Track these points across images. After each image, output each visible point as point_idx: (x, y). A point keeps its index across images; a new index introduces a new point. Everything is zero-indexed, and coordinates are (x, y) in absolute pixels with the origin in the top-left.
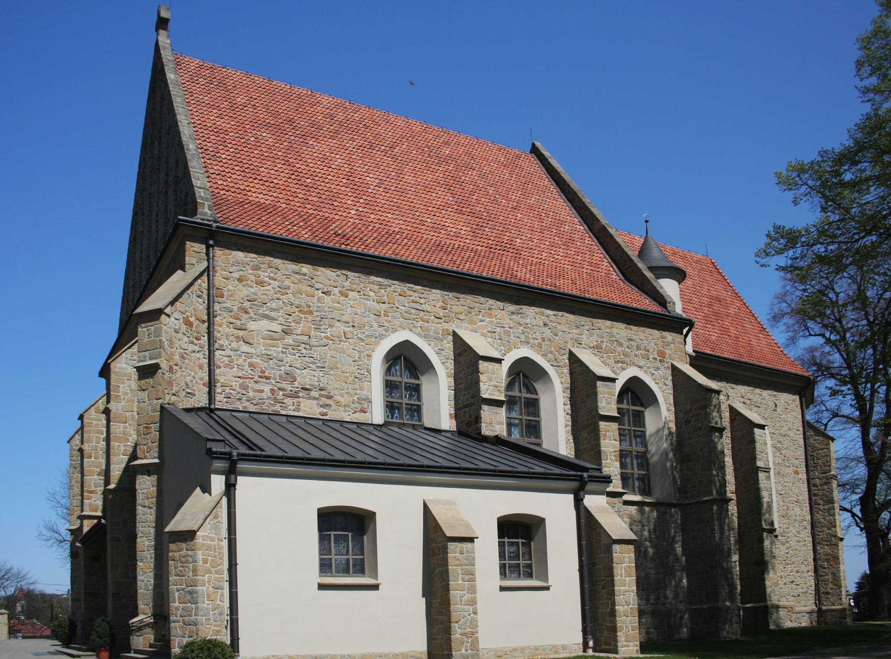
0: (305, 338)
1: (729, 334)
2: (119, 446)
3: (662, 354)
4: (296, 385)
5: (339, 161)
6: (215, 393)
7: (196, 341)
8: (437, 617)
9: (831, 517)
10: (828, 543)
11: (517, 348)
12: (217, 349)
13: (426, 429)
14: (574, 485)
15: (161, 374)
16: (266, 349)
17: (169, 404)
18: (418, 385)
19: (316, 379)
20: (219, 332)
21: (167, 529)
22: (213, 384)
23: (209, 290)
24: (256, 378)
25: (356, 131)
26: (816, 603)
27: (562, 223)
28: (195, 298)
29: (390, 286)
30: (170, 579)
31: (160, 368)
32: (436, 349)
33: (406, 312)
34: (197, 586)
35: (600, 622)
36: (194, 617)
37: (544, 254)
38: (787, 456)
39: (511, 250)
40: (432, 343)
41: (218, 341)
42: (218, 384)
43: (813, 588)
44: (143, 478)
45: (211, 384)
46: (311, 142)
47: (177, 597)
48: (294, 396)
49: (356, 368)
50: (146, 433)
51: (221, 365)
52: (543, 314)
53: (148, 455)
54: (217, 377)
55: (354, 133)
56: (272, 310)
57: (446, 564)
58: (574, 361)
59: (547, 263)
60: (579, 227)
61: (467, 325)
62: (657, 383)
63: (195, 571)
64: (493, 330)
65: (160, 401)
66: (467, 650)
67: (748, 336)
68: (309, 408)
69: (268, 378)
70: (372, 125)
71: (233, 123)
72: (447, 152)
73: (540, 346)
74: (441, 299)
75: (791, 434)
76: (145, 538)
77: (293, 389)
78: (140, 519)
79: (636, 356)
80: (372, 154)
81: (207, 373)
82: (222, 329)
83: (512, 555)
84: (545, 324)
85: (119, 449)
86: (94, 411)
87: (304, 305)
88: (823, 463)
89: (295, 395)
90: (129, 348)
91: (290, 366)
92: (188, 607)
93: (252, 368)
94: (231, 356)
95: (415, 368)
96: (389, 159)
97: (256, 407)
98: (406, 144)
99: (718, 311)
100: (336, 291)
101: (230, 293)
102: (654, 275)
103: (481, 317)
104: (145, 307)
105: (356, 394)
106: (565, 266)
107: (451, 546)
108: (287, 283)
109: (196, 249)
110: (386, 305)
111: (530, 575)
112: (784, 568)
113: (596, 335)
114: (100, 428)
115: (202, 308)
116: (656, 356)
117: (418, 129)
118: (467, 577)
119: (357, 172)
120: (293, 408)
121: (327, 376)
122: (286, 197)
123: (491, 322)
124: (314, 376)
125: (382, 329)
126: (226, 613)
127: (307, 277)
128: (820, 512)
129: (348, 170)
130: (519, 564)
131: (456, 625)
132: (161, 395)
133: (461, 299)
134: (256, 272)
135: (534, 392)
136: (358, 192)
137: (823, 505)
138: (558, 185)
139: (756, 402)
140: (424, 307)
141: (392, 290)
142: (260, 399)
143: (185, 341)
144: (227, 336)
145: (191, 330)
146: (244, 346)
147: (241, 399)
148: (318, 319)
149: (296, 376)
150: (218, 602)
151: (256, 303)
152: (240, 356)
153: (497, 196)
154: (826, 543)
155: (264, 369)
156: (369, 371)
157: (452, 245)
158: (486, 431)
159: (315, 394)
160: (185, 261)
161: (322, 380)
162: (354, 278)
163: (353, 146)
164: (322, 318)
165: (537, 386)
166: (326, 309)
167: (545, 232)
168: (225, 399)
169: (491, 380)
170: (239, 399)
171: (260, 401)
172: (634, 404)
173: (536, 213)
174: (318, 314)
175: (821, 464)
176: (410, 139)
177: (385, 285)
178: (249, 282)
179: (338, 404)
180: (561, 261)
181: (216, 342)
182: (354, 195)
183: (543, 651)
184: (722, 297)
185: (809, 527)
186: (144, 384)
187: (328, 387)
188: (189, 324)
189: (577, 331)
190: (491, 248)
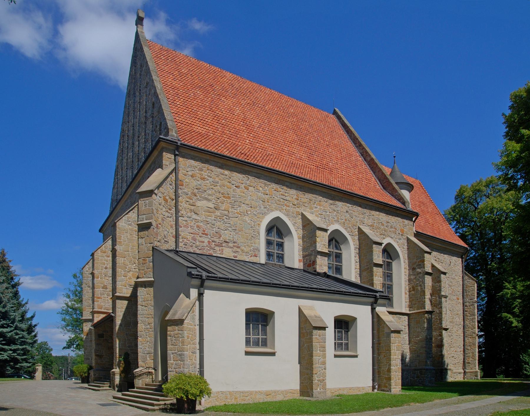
0: (226, 213)
1: (429, 222)
2: (121, 271)
3: (402, 231)
4: (221, 239)
5: (238, 111)
6: (179, 242)
7: (169, 211)
8: (304, 371)
9: (473, 323)
10: (471, 337)
11: (333, 224)
12: (180, 216)
13: (286, 267)
14: (372, 300)
15: (152, 229)
16: (206, 218)
17: (156, 247)
18: (283, 243)
19: (231, 236)
20: (181, 206)
21: (167, 318)
22: (178, 237)
24: (201, 234)
25: (245, 94)
27: (351, 155)
28: (169, 186)
30: (168, 347)
31: (152, 225)
32: (293, 222)
33: (278, 201)
34: (184, 351)
35: (381, 375)
36: (182, 369)
37: (344, 172)
38: (454, 290)
39: (328, 169)
40: (291, 219)
41: (180, 212)
42: (180, 237)
44: (142, 289)
45: (177, 236)
46: (223, 99)
47: (172, 357)
48: (220, 246)
49: (252, 231)
50: (143, 263)
51: (182, 226)
52: (346, 206)
54: (180, 233)
55: (244, 96)
56: (209, 195)
57: (312, 342)
58: (361, 232)
59: (346, 177)
60: (359, 158)
61: (308, 209)
62: (399, 247)
63: (183, 342)
64: (321, 213)
65: (152, 245)
66: (320, 389)
67: (438, 224)
68: (228, 253)
69: (207, 235)
70: (253, 92)
71: (181, 84)
72: (292, 111)
73: (344, 223)
74: (296, 194)
75: (457, 278)
76: (143, 324)
77: (220, 242)
79: (390, 231)
80: (255, 109)
81: (175, 230)
82: (183, 204)
83: (339, 338)
84: (347, 211)
85: (121, 273)
86: (100, 251)
87: (226, 194)
88: (471, 294)
89: (220, 245)
90: (127, 214)
91: (218, 228)
92: (178, 363)
93: (198, 229)
94: (187, 221)
95: (282, 234)
96: (263, 112)
98: (271, 104)
99: (423, 210)
100: (243, 186)
101: (187, 184)
102: (399, 187)
103: (315, 205)
104: (143, 188)
105: (252, 246)
106: (354, 179)
107: (315, 332)
108: (217, 179)
109: (169, 156)
110: (268, 196)
111: (347, 349)
112: (450, 349)
113: (371, 219)
114: (103, 261)
115: (172, 192)
116: (400, 232)
117: (277, 96)
118: (322, 349)
119: (248, 118)
120: (220, 252)
121: (237, 235)
122: (212, 130)
123: (320, 209)
124: (231, 234)
125: (266, 209)
126: (197, 368)
127: (227, 177)
128: (468, 320)
129: (243, 117)
130: (342, 343)
131: (316, 375)
132: (152, 242)
133: (306, 195)
134: (200, 172)
135: (339, 249)
136: (249, 130)
137: (470, 317)
138: (348, 133)
139: (441, 260)
140: (288, 198)
141: (271, 187)
142: (203, 247)
143: (164, 210)
144: (185, 209)
145: (167, 204)
146: (194, 215)
147: (192, 246)
148: (233, 202)
149: (221, 234)
150: (194, 361)
151: (200, 190)
152: (192, 221)
153: (319, 138)
154: (470, 337)
155: (204, 229)
156: (259, 233)
157: (299, 164)
158: (319, 270)
159: (231, 245)
160: (163, 163)
161: (234, 237)
162: (252, 179)
163: (244, 103)
164: (235, 201)
165: (342, 247)
166: (237, 196)
167: (343, 160)
168: (184, 246)
169: (322, 241)
170: (191, 246)
171: (202, 248)
172: (387, 259)
173: (339, 149)
174: (233, 199)
176: (273, 101)
177: (268, 184)
179: (243, 251)
180: (352, 177)
181: (179, 212)
182: (248, 132)
183: (354, 390)
184: (425, 202)
187: (238, 241)
188: (166, 201)
189: (362, 216)
190: (318, 167)
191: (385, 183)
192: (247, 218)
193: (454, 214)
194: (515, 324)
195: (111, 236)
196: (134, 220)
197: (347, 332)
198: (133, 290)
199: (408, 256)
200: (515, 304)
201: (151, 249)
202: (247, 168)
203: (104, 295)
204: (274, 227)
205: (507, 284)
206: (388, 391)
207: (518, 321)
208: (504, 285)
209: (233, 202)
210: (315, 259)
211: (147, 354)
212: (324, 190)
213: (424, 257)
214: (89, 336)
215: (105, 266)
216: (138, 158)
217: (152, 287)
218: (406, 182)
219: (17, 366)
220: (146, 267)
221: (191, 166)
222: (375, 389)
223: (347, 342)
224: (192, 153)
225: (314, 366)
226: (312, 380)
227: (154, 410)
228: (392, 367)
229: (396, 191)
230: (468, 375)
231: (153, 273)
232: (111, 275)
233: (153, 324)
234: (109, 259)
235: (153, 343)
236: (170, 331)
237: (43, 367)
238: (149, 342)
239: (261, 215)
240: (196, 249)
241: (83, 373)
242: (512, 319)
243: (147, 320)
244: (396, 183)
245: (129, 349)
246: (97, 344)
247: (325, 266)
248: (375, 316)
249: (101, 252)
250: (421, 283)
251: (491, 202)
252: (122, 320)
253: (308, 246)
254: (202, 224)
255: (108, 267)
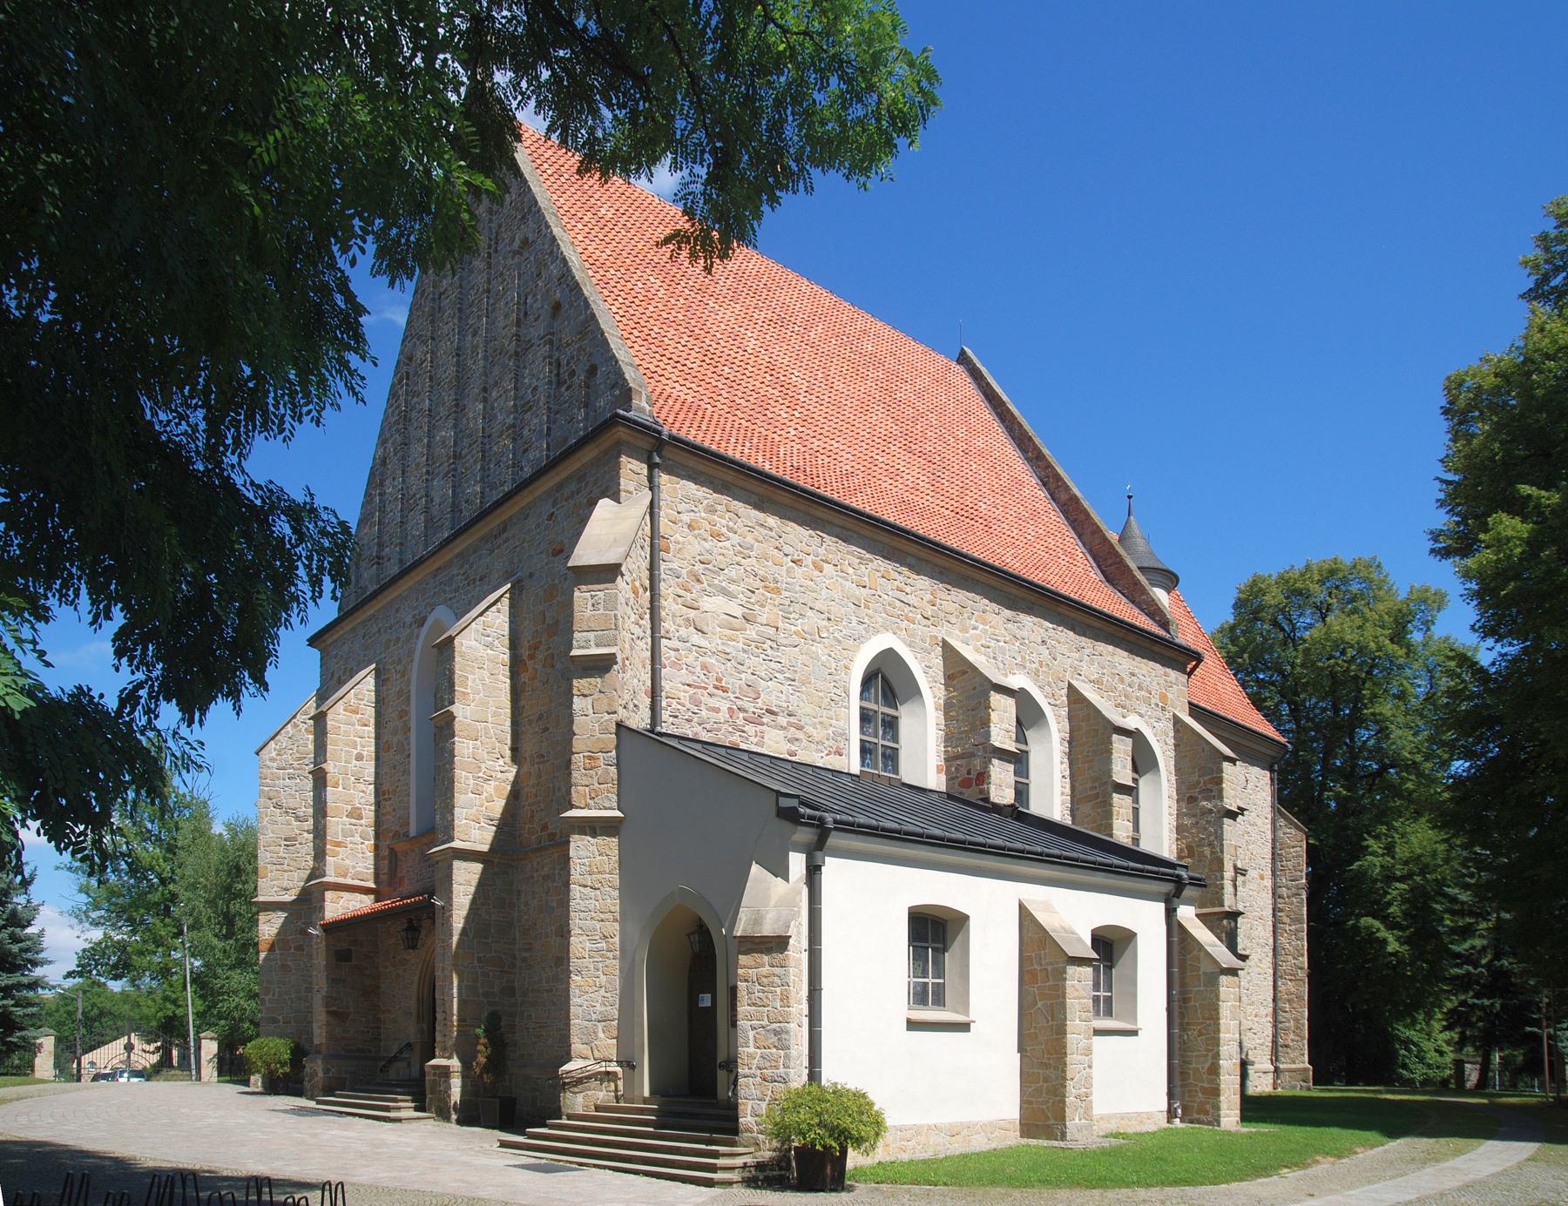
3: (1163, 698)
4: (760, 705)
14: (1168, 887)
23: (652, 538)
24: (711, 689)
26: (1271, 1060)
29: (871, 561)
33: (889, 605)
40: (919, 656)
43: (1270, 1039)
44: (583, 840)
47: (751, 1038)
49: (833, 684)
52: (1041, 626)
53: (591, 802)
57: (1064, 996)
58: (1075, 697)
66: (1080, 1120)
75: (1259, 822)
78: (577, 907)
81: (649, 675)
87: (770, 578)
89: (756, 721)
90: (481, 614)
95: (894, 696)
97: (709, 734)
100: (809, 560)
103: (973, 622)
108: (749, 539)
109: (634, 468)
110: (867, 589)
111: (940, 1001)
116: (1158, 701)
123: (985, 631)
124: (782, 692)
125: (861, 627)
127: (773, 534)
134: (710, 516)
140: (910, 599)
144: (674, 616)
159: (782, 720)
160: (619, 484)
166: (798, 588)
175: (1291, 867)
178: (702, 531)
185: (1271, 954)
186: (586, 685)
188: (635, 592)
191: (1110, 565)
192: (818, 649)
193: (1233, 649)
194: (1393, 946)
195: (374, 665)
196: (499, 631)
197: (941, 951)
198: (496, 832)
199: (1175, 766)
200: (1389, 893)
201: (613, 728)
202: (820, 513)
203: (353, 836)
204: (877, 674)
205: (1371, 842)
206: (1209, 1123)
207: (1398, 939)
208: (1365, 843)
209: (787, 602)
210: (987, 767)
211: (599, 1021)
212: (994, 581)
213: (1222, 772)
214: (277, 952)
215: (355, 752)
216: (483, 451)
217: (614, 837)
218: (1160, 566)
219: (12, 1040)
220: (596, 779)
221: (687, 499)
222: (1176, 1117)
223: (1109, 994)
224: (693, 462)
225: (1069, 1059)
226: (1064, 1096)
227: (729, 1183)
228: (1221, 1062)
229: (1144, 591)
230: (1285, 1078)
231: (618, 795)
232: (372, 779)
233: (617, 939)
234: (369, 732)
235: (618, 992)
236: (745, 967)
237: (59, 1041)
238: (603, 989)
239: (851, 642)
240: (700, 728)
241: (278, 1066)
242: (1384, 933)
243: (598, 925)
244: (1139, 568)
245: (485, 1000)
246: (333, 980)
247: (1009, 787)
248: (1175, 928)
249: (345, 710)
250: (1212, 838)
251: (1338, 628)
252: (467, 918)
253: (962, 732)
254: (713, 661)
255: (365, 753)
